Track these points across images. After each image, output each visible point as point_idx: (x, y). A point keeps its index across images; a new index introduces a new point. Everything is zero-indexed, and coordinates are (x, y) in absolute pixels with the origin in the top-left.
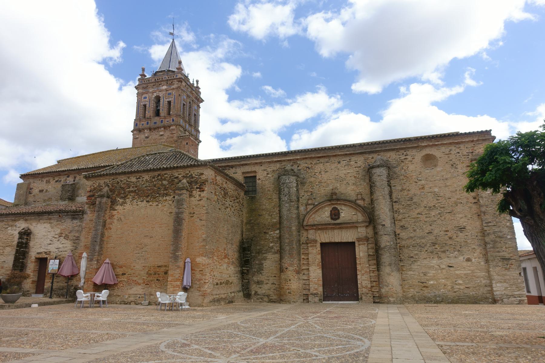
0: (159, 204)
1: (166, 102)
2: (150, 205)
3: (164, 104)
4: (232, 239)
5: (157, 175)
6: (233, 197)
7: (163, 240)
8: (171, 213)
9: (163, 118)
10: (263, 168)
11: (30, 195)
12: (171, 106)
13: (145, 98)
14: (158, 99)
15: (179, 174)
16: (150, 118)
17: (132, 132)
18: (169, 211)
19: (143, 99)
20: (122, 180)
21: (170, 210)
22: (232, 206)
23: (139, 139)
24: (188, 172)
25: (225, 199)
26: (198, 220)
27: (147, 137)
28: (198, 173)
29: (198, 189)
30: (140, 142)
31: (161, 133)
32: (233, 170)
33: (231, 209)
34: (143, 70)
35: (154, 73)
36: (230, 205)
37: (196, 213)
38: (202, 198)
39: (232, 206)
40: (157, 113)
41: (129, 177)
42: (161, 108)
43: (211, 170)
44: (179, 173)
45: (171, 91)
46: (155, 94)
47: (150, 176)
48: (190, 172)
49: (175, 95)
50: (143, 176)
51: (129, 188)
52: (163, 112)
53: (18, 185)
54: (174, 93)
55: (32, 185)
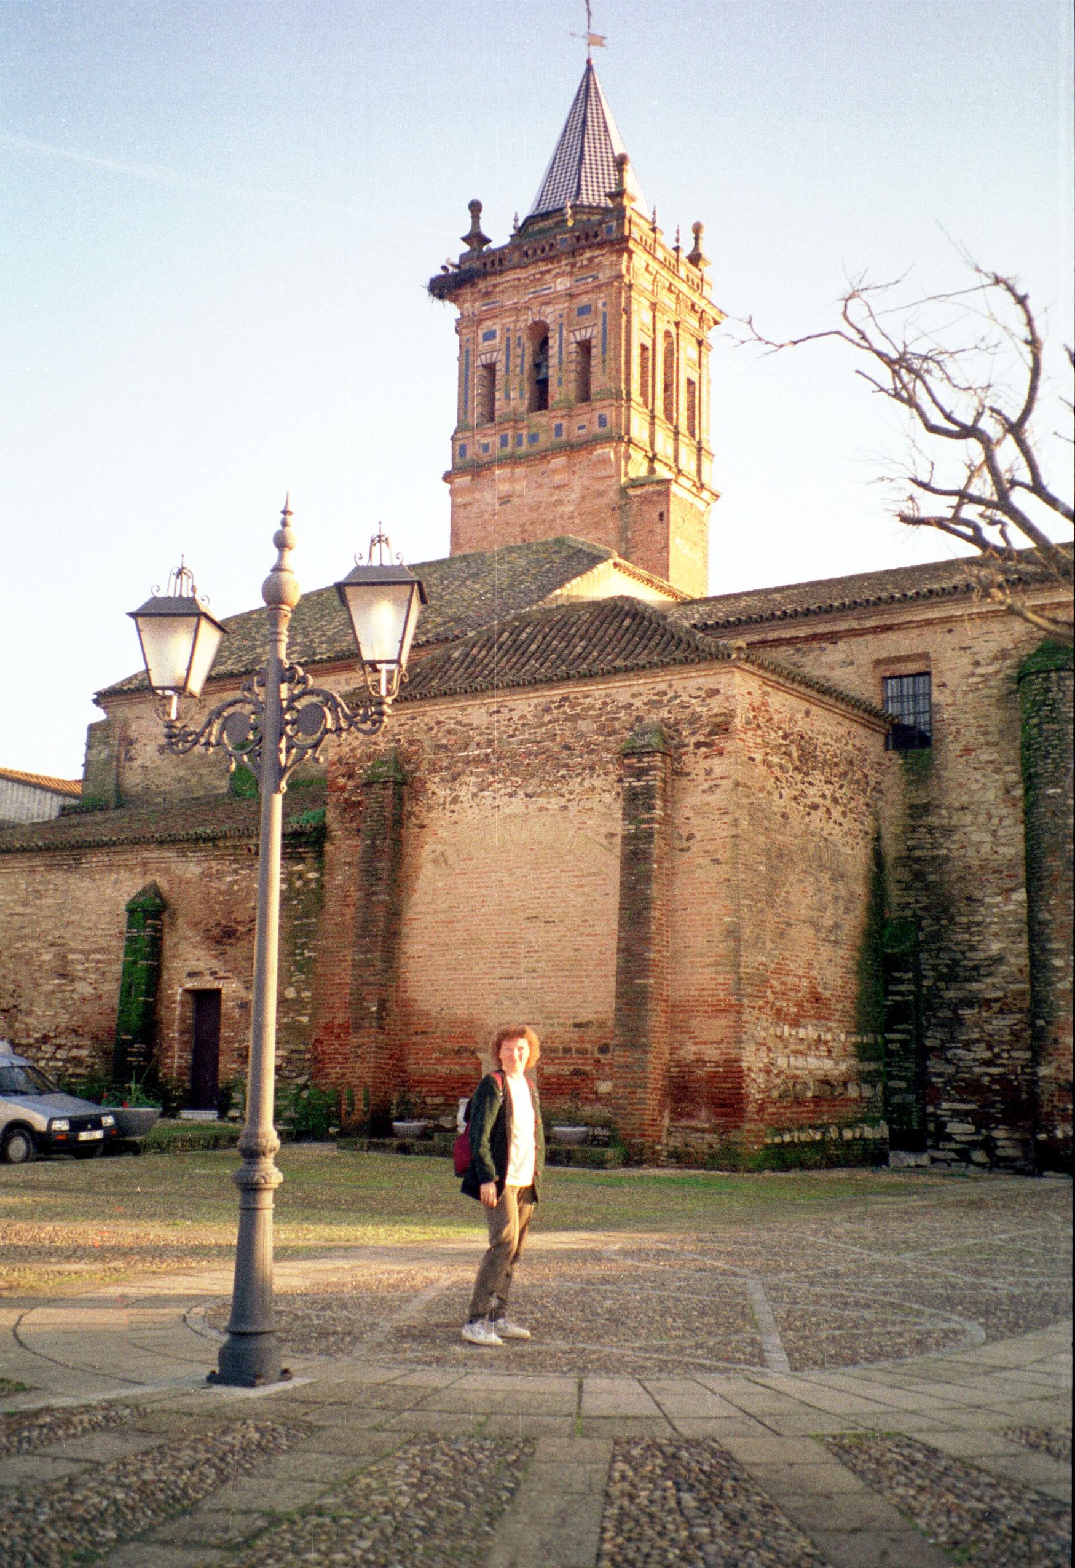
0: (569, 804)
1: (573, 347)
2: (541, 809)
3: (565, 359)
4: (837, 926)
5: (558, 698)
6: (836, 764)
7: (589, 930)
8: (612, 835)
9: (562, 417)
10: (953, 639)
11: (128, 764)
12: (593, 363)
13: (490, 336)
14: (541, 337)
15: (634, 696)
16: (515, 419)
17: (447, 477)
18: (604, 830)
19: (480, 339)
20: (442, 719)
21: (609, 824)
22: (835, 800)
23: (475, 509)
24: (662, 687)
25: (807, 774)
26: (706, 861)
27: (505, 500)
28: (700, 689)
29: (703, 749)
30: (480, 521)
31: (558, 479)
32: (836, 653)
33: (828, 811)
34: (475, 208)
35: (520, 223)
36: (823, 796)
37: (698, 836)
38: (719, 782)
39: (835, 800)
40: (541, 398)
41: (463, 709)
42: (553, 373)
43: (748, 676)
44: (635, 689)
45: (592, 296)
46: (529, 318)
47: (534, 701)
48: (671, 686)
49: (605, 315)
50: (511, 704)
51: (466, 749)
52: (560, 390)
53: (92, 728)
54: (600, 304)
55: (134, 727)
